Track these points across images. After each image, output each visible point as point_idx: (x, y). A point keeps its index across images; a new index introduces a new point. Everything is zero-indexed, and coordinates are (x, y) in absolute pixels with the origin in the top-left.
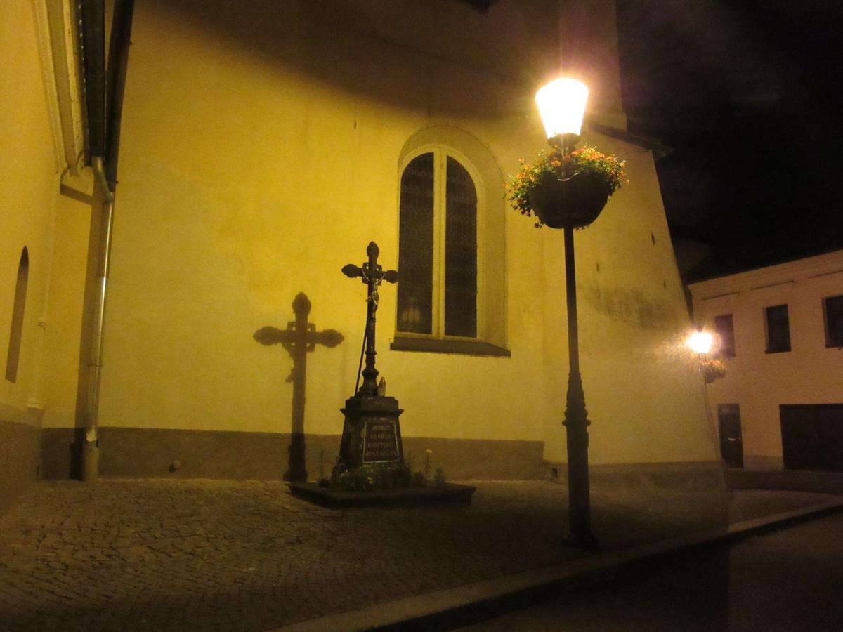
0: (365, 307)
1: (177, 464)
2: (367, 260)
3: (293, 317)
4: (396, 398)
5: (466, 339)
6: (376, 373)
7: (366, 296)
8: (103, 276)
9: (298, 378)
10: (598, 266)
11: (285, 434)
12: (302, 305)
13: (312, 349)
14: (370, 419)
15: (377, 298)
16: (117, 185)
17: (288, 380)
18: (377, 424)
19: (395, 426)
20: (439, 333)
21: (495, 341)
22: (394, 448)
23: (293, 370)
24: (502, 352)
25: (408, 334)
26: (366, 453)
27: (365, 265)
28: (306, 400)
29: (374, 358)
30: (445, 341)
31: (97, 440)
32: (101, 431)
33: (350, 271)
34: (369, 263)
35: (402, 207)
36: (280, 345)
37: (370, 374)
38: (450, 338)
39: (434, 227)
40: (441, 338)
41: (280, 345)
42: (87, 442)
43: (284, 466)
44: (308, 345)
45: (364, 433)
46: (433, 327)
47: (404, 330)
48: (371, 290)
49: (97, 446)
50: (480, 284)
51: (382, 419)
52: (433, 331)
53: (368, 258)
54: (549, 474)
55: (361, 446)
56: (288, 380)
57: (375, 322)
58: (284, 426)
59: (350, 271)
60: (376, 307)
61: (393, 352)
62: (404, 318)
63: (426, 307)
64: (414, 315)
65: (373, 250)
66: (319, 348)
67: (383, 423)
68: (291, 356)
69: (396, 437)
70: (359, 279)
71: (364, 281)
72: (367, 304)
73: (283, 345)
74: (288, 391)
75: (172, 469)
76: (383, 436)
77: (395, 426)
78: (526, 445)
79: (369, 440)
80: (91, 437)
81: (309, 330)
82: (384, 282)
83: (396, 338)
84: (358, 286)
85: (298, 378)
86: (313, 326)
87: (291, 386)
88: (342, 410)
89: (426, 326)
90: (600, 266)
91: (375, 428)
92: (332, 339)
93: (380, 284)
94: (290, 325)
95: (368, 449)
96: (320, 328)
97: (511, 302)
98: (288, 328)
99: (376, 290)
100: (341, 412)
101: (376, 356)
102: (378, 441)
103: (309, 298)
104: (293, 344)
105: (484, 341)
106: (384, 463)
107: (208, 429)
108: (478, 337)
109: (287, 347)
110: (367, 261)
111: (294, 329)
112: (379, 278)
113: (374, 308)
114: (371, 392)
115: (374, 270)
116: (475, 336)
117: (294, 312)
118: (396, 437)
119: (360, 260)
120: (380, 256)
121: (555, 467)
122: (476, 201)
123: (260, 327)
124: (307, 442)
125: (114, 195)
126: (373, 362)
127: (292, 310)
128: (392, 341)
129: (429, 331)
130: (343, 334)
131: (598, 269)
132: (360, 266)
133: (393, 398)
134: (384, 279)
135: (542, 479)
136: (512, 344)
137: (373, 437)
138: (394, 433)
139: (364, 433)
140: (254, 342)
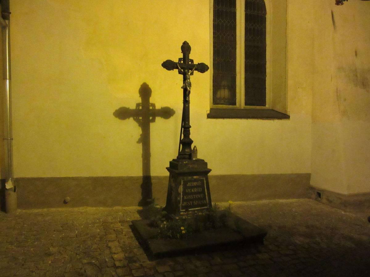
0: (181, 93)
1: (68, 198)
2: (181, 56)
3: (139, 100)
4: (206, 161)
5: (258, 107)
6: (191, 142)
7: (181, 84)
8: (7, 79)
9: (145, 140)
10: (356, 52)
11: (138, 177)
12: (145, 91)
13: (153, 120)
14: (185, 178)
15: (190, 85)
16: (10, 15)
17: (138, 142)
18: (191, 181)
19: (205, 182)
20: (241, 105)
21: (278, 108)
22: (205, 198)
23: (141, 135)
24: (284, 116)
25: (220, 106)
26: (183, 203)
27: (180, 60)
28: (151, 154)
29: (189, 131)
30: (245, 110)
31: (15, 187)
32: (17, 181)
33: (168, 65)
34: (183, 58)
35: (214, 20)
36: (131, 119)
37: (186, 142)
38: (249, 107)
39: (237, 37)
40: (242, 108)
41: (131, 119)
42: (6, 189)
43: (138, 196)
44: (151, 118)
45: (181, 189)
46: (237, 100)
47: (218, 104)
48: (185, 79)
49: (15, 191)
50: (268, 70)
51: (195, 177)
52: (237, 104)
53: (182, 54)
54: (314, 196)
55: (179, 199)
56: (138, 142)
57: (189, 103)
58: (137, 172)
59: (168, 65)
60: (189, 92)
61: (210, 120)
62: (218, 95)
63: (232, 88)
64: (224, 93)
65: (186, 48)
66: (158, 119)
67: (195, 180)
68: (139, 125)
69: (206, 190)
70: (176, 71)
71: (180, 73)
72: (182, 90)
73: (135, 120)
74: (139, 148)
75: (65, 202)
76: (196, 190)
77: (205, 182)
78: (299, 176)
79: (185, 193)
80: (9, 185)
81: (151, 108)
82: (196, 72)
83: (211, 109)
84: (176, 77)
85: (145, 140)
86: (153, 105)
87: (140, 146)
88: (167, 168)
89: (232, 100)
90: (354, 54)
91: (189, 184)
92: (167, 113)
93: (192, 74)
94: (138, 105)
95: (184, 200)
96: (158, 106)
97: (290, 82)
98: (137, 107)
99: (189, 79)
100: (167, 170)
101: (190, 129)
102: (192, 193)
103: (150, 86)
104: (141, 118)
105: (271, 109)
106: (197, 210)
107: (88, 176)
108: (267, 106)
109: (137, 120)
110: (182, 57)
111: (141, 108)
112: (191, 69)
113: (187, 92)
114: (187, 156)
115: (187, 63)
116: (265, 105)
117: (140, 96)
118: (206, 190)
119: (176, 56)
120: (192, 52)
121: (319, 192)
122: (265, 14)
123: (117, 108)
124: (153, 181)
125: (9, 22)
126: (189, 134)
127: (138, 95)
128: (208, 112)
129: (234, 104)
130: (174, 109)
131: (356, 55)
132: (176, 60)
133: (203, 161)
134: (196, 70)
135: (310, 198)
136: (290, 112)
137: (188, 191)
138: (194, 210)
139: (181, 189)
140: (113, 117)
